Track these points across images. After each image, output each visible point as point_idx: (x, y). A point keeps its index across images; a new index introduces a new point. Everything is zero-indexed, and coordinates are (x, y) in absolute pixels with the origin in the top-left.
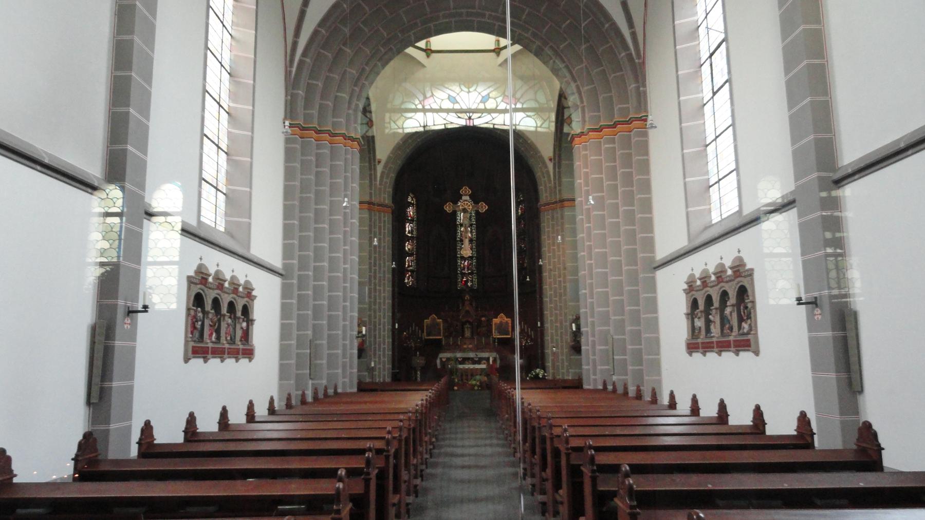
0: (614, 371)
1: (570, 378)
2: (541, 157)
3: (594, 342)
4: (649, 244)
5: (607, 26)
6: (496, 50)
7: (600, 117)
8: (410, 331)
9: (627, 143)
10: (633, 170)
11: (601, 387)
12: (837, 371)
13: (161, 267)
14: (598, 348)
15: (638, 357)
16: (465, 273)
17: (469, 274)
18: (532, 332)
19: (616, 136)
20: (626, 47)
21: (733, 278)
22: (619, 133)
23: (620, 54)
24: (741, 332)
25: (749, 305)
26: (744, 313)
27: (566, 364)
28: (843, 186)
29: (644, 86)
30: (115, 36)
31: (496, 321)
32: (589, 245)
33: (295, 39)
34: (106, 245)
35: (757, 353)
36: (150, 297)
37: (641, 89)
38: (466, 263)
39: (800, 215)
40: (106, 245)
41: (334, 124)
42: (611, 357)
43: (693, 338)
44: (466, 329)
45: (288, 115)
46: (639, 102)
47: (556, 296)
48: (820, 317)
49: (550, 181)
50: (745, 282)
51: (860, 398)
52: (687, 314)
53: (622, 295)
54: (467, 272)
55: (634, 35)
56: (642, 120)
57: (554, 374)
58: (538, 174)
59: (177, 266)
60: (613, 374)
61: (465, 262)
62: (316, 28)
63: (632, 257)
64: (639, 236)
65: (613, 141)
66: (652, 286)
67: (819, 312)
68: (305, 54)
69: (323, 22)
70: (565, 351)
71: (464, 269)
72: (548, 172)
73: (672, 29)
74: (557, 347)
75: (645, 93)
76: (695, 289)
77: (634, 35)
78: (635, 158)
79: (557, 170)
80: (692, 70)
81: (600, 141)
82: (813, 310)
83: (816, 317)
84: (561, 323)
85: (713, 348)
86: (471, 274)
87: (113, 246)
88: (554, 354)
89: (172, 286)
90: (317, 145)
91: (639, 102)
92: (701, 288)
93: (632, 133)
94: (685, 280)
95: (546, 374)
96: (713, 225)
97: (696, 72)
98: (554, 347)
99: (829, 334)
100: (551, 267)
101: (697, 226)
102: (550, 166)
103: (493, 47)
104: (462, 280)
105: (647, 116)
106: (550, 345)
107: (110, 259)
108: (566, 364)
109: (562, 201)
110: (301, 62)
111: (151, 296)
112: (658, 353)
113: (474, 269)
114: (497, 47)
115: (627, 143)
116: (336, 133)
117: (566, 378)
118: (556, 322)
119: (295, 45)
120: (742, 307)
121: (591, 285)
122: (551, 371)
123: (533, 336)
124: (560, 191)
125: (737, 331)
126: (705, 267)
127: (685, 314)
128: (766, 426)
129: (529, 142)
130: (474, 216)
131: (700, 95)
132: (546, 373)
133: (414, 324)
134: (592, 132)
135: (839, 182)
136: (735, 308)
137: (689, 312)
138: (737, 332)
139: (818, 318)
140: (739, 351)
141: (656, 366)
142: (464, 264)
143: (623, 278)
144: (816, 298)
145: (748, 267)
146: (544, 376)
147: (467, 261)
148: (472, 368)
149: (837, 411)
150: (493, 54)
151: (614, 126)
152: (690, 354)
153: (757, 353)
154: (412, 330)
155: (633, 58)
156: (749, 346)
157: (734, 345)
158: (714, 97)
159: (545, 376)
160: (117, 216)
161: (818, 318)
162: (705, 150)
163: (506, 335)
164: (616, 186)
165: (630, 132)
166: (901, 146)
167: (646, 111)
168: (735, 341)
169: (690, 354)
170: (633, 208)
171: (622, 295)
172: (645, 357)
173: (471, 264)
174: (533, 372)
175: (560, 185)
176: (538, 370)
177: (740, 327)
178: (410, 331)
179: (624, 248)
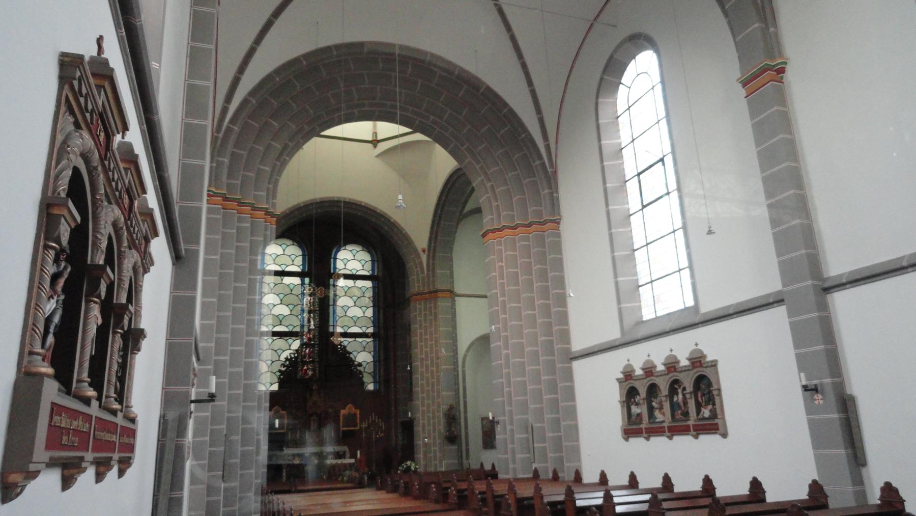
0: (534, 459)
1: (444, 470)
2: (416, 250)
3: (512, 430)
4: (565, 336)
5: (523, 136)
6: (374, 142)
7: (513, 216)
8: (370, 420)
9: (541, 242)
10: (548, 267)
11: (551, 475)
12: (846, 448)
13: (353, 339)
14: (517, 436)
15: (558, 445)
16: (306, 361)
17: (310, 362)
18: (383, 424)
19: (530, 235)
20: (540, 157)
21: (691, 368)
22: (550, 230)
23: (534, 162)
24: (700, 416)
25: (715, 393)
26: (702, 399)
27: (438, 455)
28: (832, 293)
29: (557, 192)
30: (187, 79)
31: (343, 412)
32: (505, 335)
33: (225, 105)
34: (284, 310)
35: (725, 435)
36: (361, 376)
37: (555, 195)
38: (307, 351)
39: (790, 314)
40: (284, 310)
41: (255, 197)
42: (531, 446)
43: (650, 423)
44: (312, 422)
45: (213, 183)
46: (553, 205)
47: (428, 386)
48: (821, 402)
49: (423, 272)
50: (708, 372)
51: (864, 471)
52: (622, 402)
53: (540, 384)
54: (308, 360)
55: (548, 147)
56: (556, 223)
57: (426, 466)
58: (410, 265)
59: (371, 339)
60: (534, 462)
61: (306, 349)
62: (246, 96)
63: (549, 349)
64: (556, 328)
65: (527, 239)
66: (569, 376)
67: (820, 397)
68: (233, 120)
69: (253, 93)
70: (438, 441)
71: (305, 357)
72: (421, 263)
73: (597, 150)
74: (429, 437)
75: (558, 198)
76: (634, 378)
77: (548, 147)
78: (549, 257)
79: (431, 261)
80: (618, 185)
81: (515, 239)
82: (812, 396)
83: (816, 402)
84: (433, 413)
85: (665, 432)
86: (313, 362)
87: (294, 312)
88: (426, 445)
89: (368, 363)
90: (239, 218)
91: (553, 205)
92: (644, 377)
93: (545, 234)
94: (622, 370)
95: (417, 467)
96: (643, 322)
97: (621, 186)
98: (426, 438)
99: (836, 416)
100: (424, 356)
101: (629, 321)
102: (424, 258)
103: (370, 139)
104: (302, 369)
105: (560, 219)
106: (422, 436)
107: (290, 329)
108: (438, 455)
109: (436, 291)
110: (229, 130)
111: (362, 375)
112: (577, 440)
113: (316, 357)
114: (375, 139)
115: (541, 242)
116: (258, 207)
117: (439, 469)
118: (428, 412)
119: (225, 110)
120: (699, 395)
121: (508, 374)
122: (422, 462)
123: (383, 428)
124: (434, 281)
125: (695, 415)
126: (647, 358)
127: (620, 402)
128: (828, 498)
129: (403, 232)
130: (317, 302)
131: (627, 206)
132: (417, 465)
133: (373, 414)
134: (508, 229)
135: (827, 290)
136: (693, 395)
137: (624, 399)
138: (696, 417)
139: (819, 403)
140: (698, 434)
141: (576, 451)
142: (305, 351)
143: (541, 367)
144: (816, 385)
145: (710, 358)
146: (416, 469)
147: (308, 349)
148: (339, 463)
149: (850, 482)
150: (370, 145)
151: (530, 225)
152: (627, 439)
153: (725, 435)
154: (372, 419)
155: (546, 167)
156: (718, 429)
157: (693, 429)
158: (644, 210)
159: (417, 469)
160: (369, 280)
161: (819, 403)
162: (633, 254)
163: (354, 427)
164: (531, 281)
165: (544, 232)
166: (904, 264)
167: (559, 215)
168: (646, 428)
169: (627, 439)
170: (549, 302)
171: (540, 384)
172: (564, 444)
173: (312, 352)
174: (403, 464)
175: (433, 276)
176: (409, 463)
177: (698, 411)
178: (370, 420)
179: (541, 339)
